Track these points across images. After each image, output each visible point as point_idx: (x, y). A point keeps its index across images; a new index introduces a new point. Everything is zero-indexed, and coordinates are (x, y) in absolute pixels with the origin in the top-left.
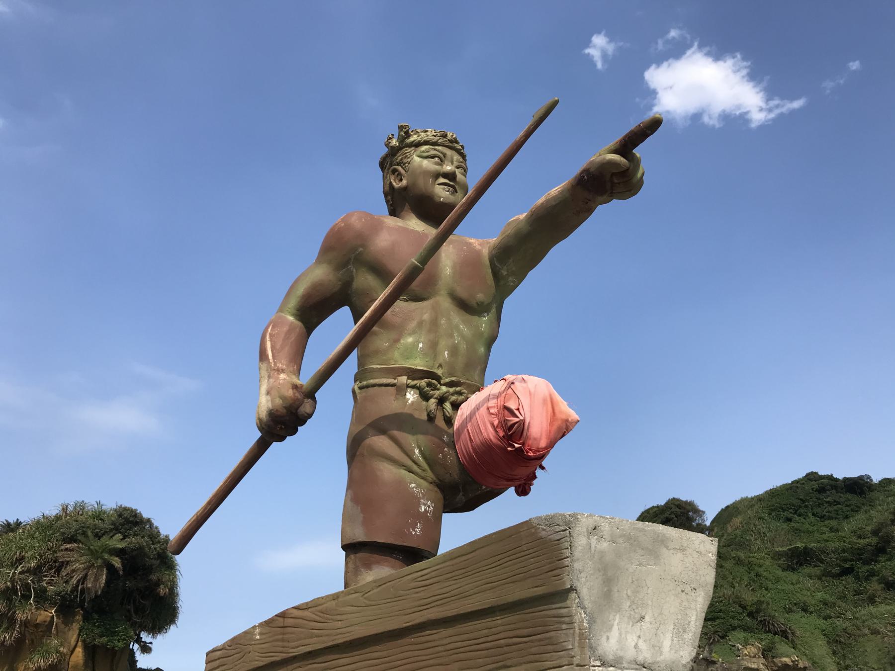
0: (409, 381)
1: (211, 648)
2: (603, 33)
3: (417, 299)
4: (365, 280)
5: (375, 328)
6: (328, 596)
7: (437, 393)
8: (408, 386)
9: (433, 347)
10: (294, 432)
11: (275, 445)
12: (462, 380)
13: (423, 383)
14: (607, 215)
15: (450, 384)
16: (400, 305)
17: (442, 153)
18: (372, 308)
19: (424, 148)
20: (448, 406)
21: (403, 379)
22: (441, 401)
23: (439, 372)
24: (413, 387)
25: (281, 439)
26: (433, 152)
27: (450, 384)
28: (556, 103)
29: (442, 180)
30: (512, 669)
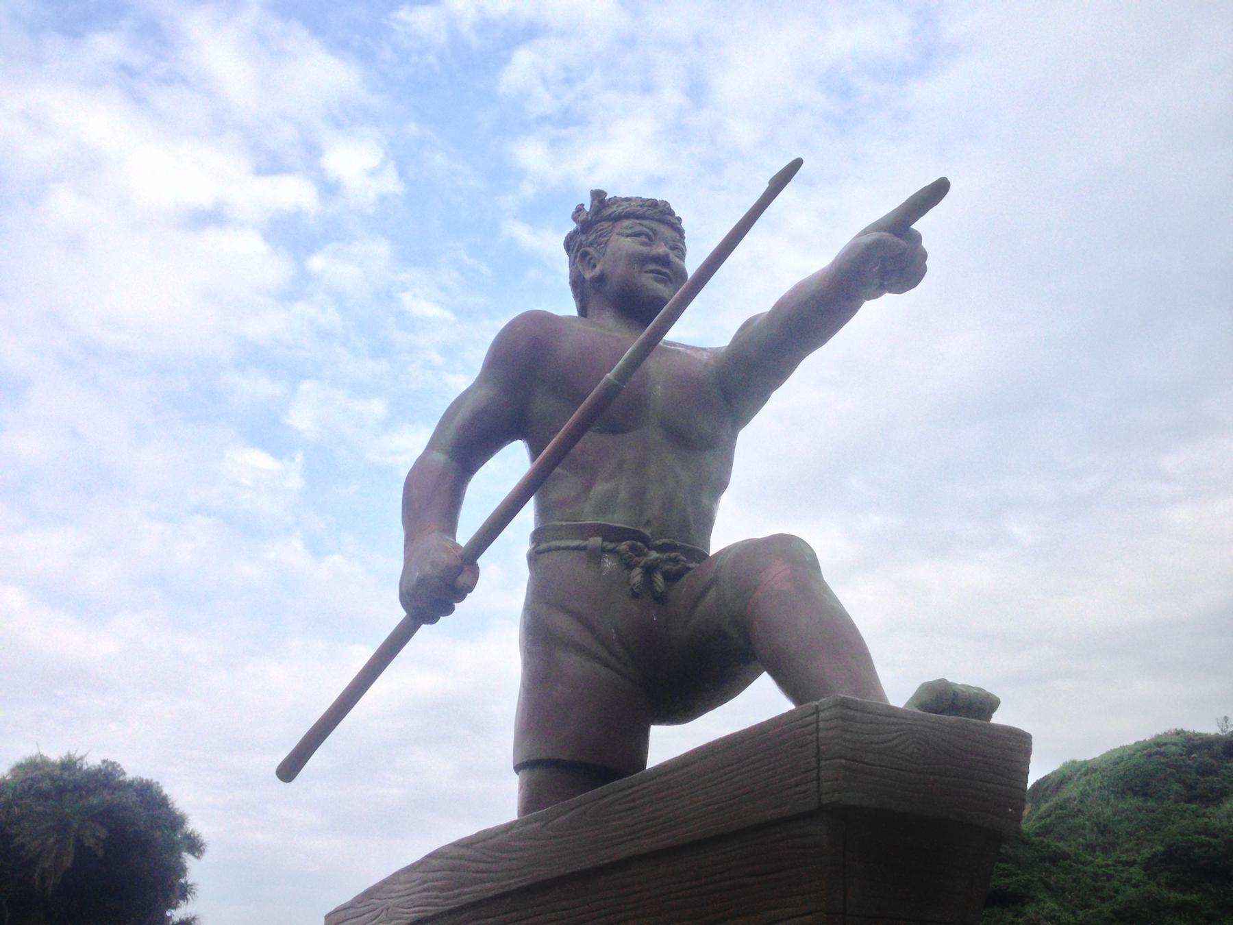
0: (605, 544)
1: (331, 909)
2: (183, 881)
3: (615, 429)
4: (542, 404)
5: (557, 470)
6: (498, 828)
7: (643, 561)
8: (603, 550)
9: (639, 496)
10: (449, 610)
11: (424, 629)
12: (679, 543)
13: (623, 546)
14: (877, 314)
15: (662, 549)
16: (591, 439)
17: (652, 230)
18: (625, 356)
19: (626, 223)
20: (659, 579)
21: (596, 541)
22: (649, 570)
23: (648, 532)
24: (612, 551)
25: (432, 619)
26: (638, 229)
27: (662, 549)
28: (796, 165)
29: (652, 267)
30: (762, 187)
